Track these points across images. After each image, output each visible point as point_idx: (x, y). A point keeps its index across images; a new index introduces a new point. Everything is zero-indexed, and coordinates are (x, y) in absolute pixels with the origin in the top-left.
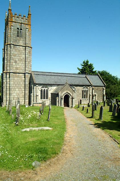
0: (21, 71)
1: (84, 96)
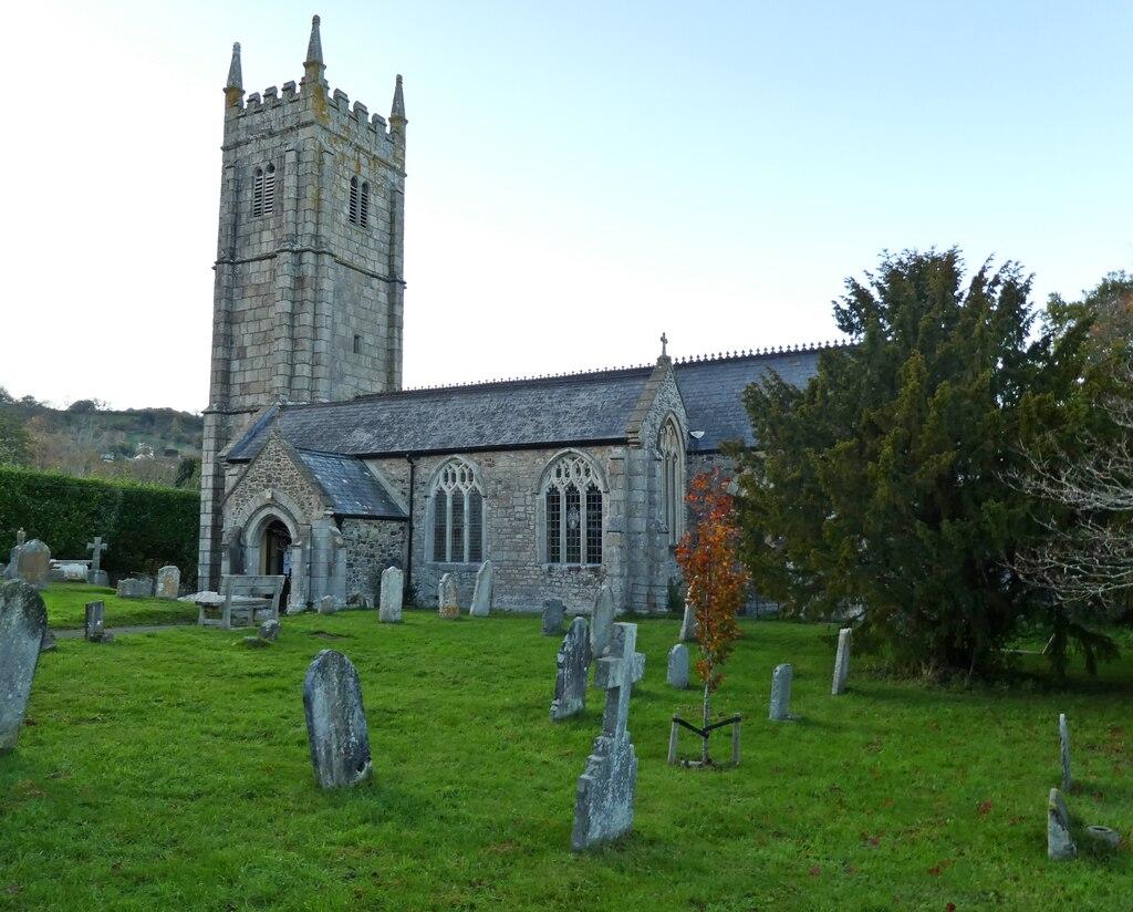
1: (563, 538)
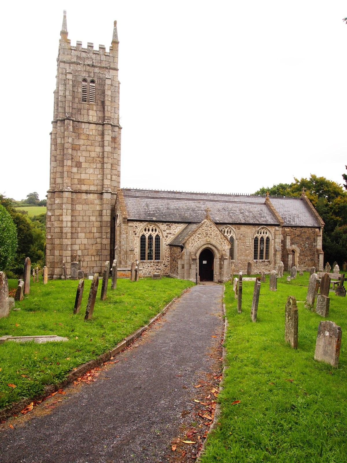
0: (93, 188)
1: (259, 252)
